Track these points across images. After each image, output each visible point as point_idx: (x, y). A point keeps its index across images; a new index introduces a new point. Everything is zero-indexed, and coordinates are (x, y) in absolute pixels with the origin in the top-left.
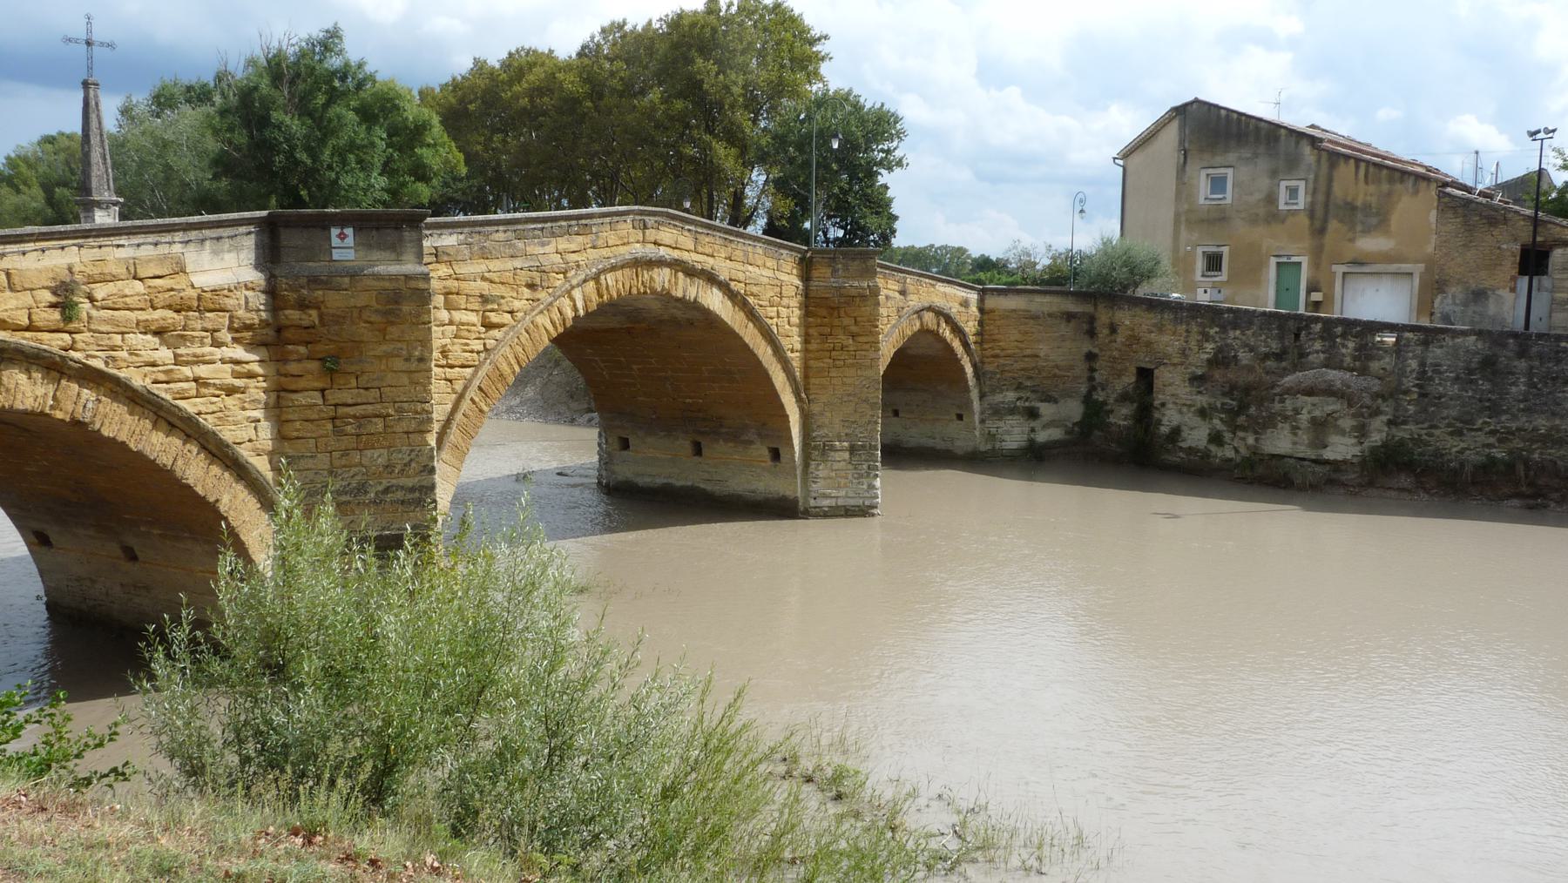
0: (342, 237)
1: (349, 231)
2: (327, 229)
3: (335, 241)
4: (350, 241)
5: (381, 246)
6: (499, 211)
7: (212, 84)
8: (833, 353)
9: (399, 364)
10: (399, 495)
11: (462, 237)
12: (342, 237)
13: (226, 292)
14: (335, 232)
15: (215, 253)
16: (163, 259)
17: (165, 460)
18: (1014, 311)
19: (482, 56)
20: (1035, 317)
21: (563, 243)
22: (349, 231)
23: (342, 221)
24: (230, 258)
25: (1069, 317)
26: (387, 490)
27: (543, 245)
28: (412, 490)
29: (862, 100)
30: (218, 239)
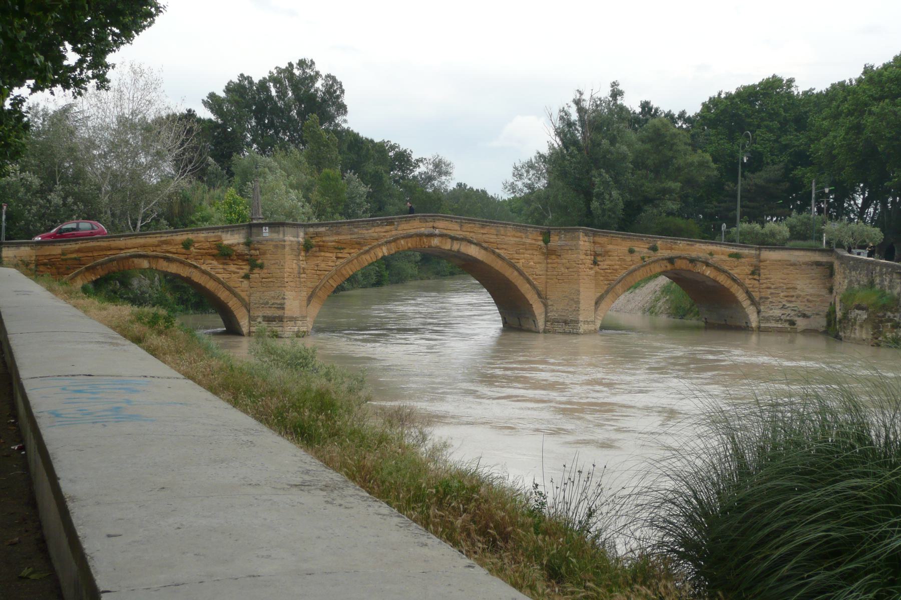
0: (266, 230)
1: (267, 228)
2: (262, 227)
3: (264, 231)
4: (267, 231)
5: (275, 232)
6: (731, 214)
7: (676, 116)
8: (558, 277)
9: (276, 266)
10: (276, 306)
11: (327, 228)
12: (266, 230)
13: (801, 323)
14: (264, 228)
15: (231, 235)
16: (215, 237)
17: (212, 289)
18: (780, 261)
19: (870, 62)
20: (793, 265)
21: (378, 229)
22: (267, 228)
23: (265, 225)
24: (236, 236)
25: (818, 264)
26: (273, 304)
27: (367, 230)
28: (279, 304)
29: (545, 151)
30: (233, 230)
